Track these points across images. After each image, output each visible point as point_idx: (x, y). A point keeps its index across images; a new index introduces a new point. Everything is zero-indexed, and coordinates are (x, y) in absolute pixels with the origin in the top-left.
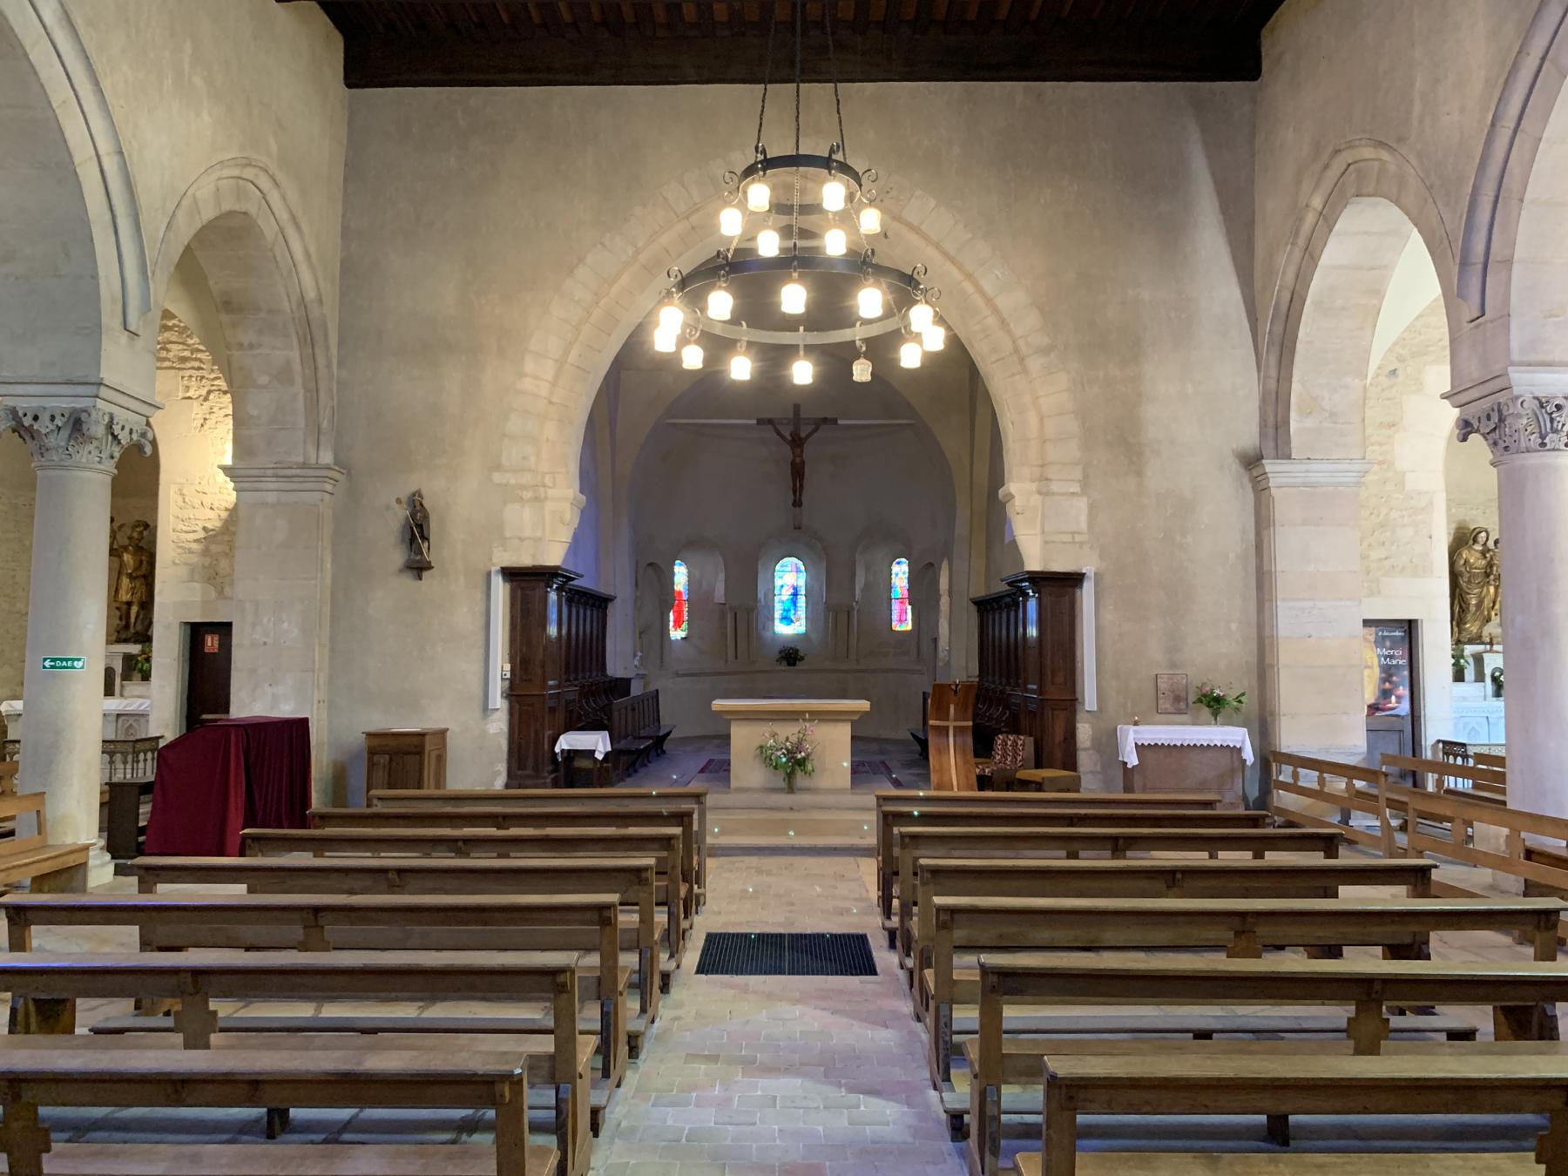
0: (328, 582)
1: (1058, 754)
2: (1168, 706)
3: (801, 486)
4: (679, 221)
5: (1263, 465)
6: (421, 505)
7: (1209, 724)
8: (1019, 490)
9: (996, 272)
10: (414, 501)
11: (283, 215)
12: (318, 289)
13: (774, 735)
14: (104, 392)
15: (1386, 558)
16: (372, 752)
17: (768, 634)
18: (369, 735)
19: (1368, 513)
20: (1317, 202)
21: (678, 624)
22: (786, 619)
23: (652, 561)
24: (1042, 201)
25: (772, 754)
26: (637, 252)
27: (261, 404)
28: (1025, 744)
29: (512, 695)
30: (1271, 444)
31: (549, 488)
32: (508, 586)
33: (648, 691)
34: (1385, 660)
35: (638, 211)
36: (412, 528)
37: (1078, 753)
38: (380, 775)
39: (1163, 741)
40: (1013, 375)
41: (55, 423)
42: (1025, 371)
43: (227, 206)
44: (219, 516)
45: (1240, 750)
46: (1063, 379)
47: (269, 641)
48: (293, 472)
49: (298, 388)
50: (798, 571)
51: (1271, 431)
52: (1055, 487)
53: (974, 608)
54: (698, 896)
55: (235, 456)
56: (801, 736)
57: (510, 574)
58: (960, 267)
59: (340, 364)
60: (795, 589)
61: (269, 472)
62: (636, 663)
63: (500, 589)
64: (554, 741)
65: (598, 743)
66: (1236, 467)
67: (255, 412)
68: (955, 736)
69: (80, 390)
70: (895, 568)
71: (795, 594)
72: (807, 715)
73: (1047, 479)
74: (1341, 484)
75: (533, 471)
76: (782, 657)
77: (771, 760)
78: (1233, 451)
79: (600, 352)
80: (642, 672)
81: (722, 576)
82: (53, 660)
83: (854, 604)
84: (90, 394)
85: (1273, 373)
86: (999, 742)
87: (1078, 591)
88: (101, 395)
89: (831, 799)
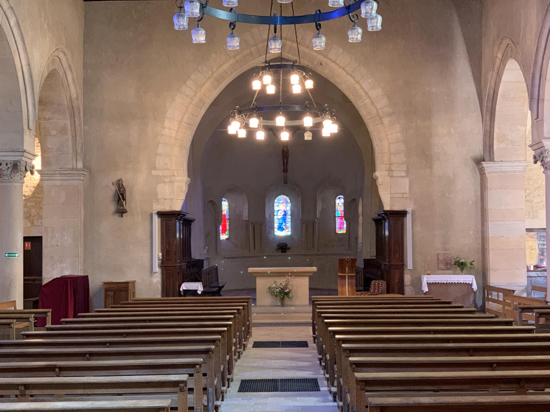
0: (83, 219)
1: (396, 288)
2: (443, 267)
3: (287, 162)
4: (231, 59)
5: (482, 164)
6: (122, 185)
7: (459, 274)
8: (380, 174)
9: (369, 80)
10: (119, 183)
11: (66, 65)
12: (77, 93)
13: (275, 282)
14: (25, 154)
15: (541, 202)
16: (107, 290)
17: (272, 236)
18: (105, 283)
19: (533, 182)
20: (500, 55)
21: (224, 231)
22: (281, 228)
23: (212, 200)
24: (389, 49)
25: (274, 290)
26: (213, 73)
27: (52, 143)
28: (383, 284)
29: (162, 266)
30: (488, 154)
31: (176, 176)
32: (160, 219)
33: (210, 266)
34: (541, 246)
35: (213, 55)
36: (119, 195)
37: (405, 287)
38: (110, 300)
39: (439, 281)
40: (377, 125)
41: (8, 166)
42: (382, 123)
43: (50, 69)
44: (31, 190)
45: (472, 284)
46: (398, 127)
47: (59, 244)
48: (68, 172)
49: (69, 136)
50: (287, 202)
51: (488, 149)
52: (395, 174)
53: (373, 223)
54: (244, 345)
55: (42, 166)
56: (287, 282)
57: (161, 214)
58: (354, 78)
59: (85, 124)
60: (285, 212)
61: (57, 172)
62: (205, 252)
63: (157, 221)
64: (180, 286)
65: (199, 287)
66: (472, 164)
67: (50, 147)
68: (348, 280)
69: (17, 154)
70: (338, 201)
71: (285, 215)
72: (289, 274)
73: (392, 170)
74: (516, 171)
75: (169, 169)
76: (279, 248)
77: (274, 293)
78: (471, 157)
79: (197, 116)
80: (208, 257)
81: (246, 206)
82: (9, 254)
83: (316, 220)
84: (20, 155)
85: (488, 123)
86: (373, 284)
87: (405, 218)
88: (24, 155)
89: (300, 309)
